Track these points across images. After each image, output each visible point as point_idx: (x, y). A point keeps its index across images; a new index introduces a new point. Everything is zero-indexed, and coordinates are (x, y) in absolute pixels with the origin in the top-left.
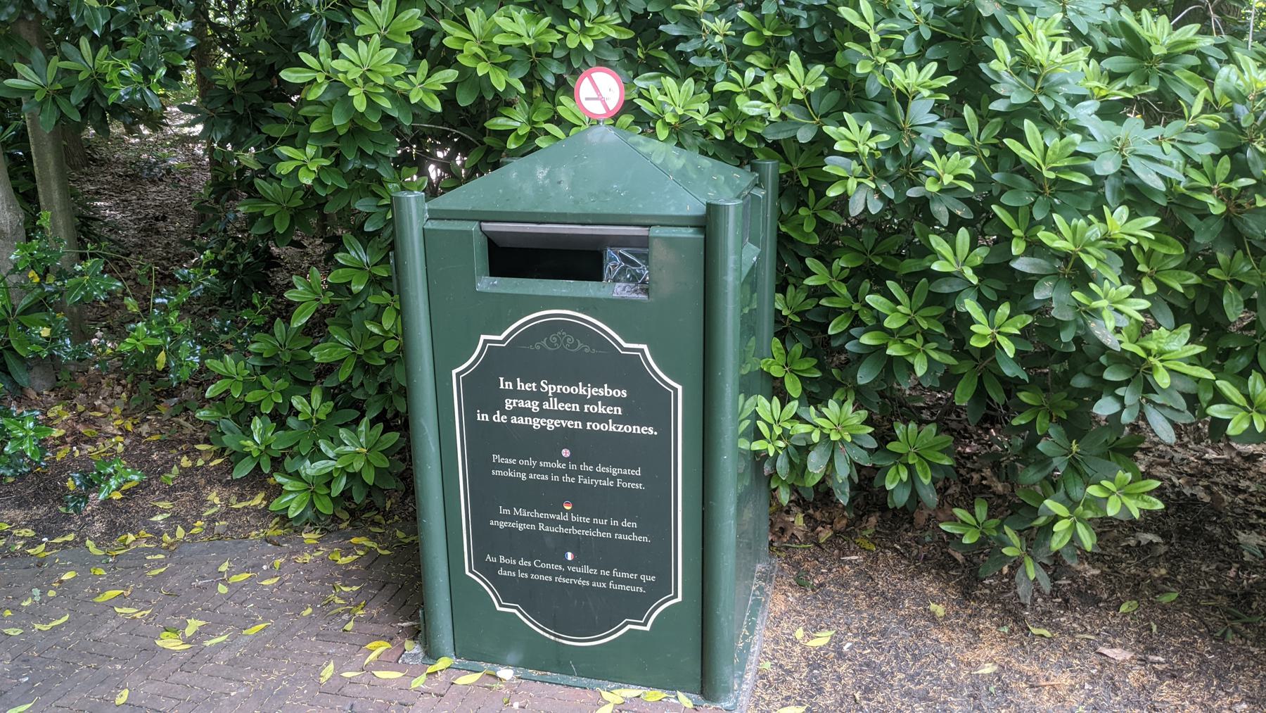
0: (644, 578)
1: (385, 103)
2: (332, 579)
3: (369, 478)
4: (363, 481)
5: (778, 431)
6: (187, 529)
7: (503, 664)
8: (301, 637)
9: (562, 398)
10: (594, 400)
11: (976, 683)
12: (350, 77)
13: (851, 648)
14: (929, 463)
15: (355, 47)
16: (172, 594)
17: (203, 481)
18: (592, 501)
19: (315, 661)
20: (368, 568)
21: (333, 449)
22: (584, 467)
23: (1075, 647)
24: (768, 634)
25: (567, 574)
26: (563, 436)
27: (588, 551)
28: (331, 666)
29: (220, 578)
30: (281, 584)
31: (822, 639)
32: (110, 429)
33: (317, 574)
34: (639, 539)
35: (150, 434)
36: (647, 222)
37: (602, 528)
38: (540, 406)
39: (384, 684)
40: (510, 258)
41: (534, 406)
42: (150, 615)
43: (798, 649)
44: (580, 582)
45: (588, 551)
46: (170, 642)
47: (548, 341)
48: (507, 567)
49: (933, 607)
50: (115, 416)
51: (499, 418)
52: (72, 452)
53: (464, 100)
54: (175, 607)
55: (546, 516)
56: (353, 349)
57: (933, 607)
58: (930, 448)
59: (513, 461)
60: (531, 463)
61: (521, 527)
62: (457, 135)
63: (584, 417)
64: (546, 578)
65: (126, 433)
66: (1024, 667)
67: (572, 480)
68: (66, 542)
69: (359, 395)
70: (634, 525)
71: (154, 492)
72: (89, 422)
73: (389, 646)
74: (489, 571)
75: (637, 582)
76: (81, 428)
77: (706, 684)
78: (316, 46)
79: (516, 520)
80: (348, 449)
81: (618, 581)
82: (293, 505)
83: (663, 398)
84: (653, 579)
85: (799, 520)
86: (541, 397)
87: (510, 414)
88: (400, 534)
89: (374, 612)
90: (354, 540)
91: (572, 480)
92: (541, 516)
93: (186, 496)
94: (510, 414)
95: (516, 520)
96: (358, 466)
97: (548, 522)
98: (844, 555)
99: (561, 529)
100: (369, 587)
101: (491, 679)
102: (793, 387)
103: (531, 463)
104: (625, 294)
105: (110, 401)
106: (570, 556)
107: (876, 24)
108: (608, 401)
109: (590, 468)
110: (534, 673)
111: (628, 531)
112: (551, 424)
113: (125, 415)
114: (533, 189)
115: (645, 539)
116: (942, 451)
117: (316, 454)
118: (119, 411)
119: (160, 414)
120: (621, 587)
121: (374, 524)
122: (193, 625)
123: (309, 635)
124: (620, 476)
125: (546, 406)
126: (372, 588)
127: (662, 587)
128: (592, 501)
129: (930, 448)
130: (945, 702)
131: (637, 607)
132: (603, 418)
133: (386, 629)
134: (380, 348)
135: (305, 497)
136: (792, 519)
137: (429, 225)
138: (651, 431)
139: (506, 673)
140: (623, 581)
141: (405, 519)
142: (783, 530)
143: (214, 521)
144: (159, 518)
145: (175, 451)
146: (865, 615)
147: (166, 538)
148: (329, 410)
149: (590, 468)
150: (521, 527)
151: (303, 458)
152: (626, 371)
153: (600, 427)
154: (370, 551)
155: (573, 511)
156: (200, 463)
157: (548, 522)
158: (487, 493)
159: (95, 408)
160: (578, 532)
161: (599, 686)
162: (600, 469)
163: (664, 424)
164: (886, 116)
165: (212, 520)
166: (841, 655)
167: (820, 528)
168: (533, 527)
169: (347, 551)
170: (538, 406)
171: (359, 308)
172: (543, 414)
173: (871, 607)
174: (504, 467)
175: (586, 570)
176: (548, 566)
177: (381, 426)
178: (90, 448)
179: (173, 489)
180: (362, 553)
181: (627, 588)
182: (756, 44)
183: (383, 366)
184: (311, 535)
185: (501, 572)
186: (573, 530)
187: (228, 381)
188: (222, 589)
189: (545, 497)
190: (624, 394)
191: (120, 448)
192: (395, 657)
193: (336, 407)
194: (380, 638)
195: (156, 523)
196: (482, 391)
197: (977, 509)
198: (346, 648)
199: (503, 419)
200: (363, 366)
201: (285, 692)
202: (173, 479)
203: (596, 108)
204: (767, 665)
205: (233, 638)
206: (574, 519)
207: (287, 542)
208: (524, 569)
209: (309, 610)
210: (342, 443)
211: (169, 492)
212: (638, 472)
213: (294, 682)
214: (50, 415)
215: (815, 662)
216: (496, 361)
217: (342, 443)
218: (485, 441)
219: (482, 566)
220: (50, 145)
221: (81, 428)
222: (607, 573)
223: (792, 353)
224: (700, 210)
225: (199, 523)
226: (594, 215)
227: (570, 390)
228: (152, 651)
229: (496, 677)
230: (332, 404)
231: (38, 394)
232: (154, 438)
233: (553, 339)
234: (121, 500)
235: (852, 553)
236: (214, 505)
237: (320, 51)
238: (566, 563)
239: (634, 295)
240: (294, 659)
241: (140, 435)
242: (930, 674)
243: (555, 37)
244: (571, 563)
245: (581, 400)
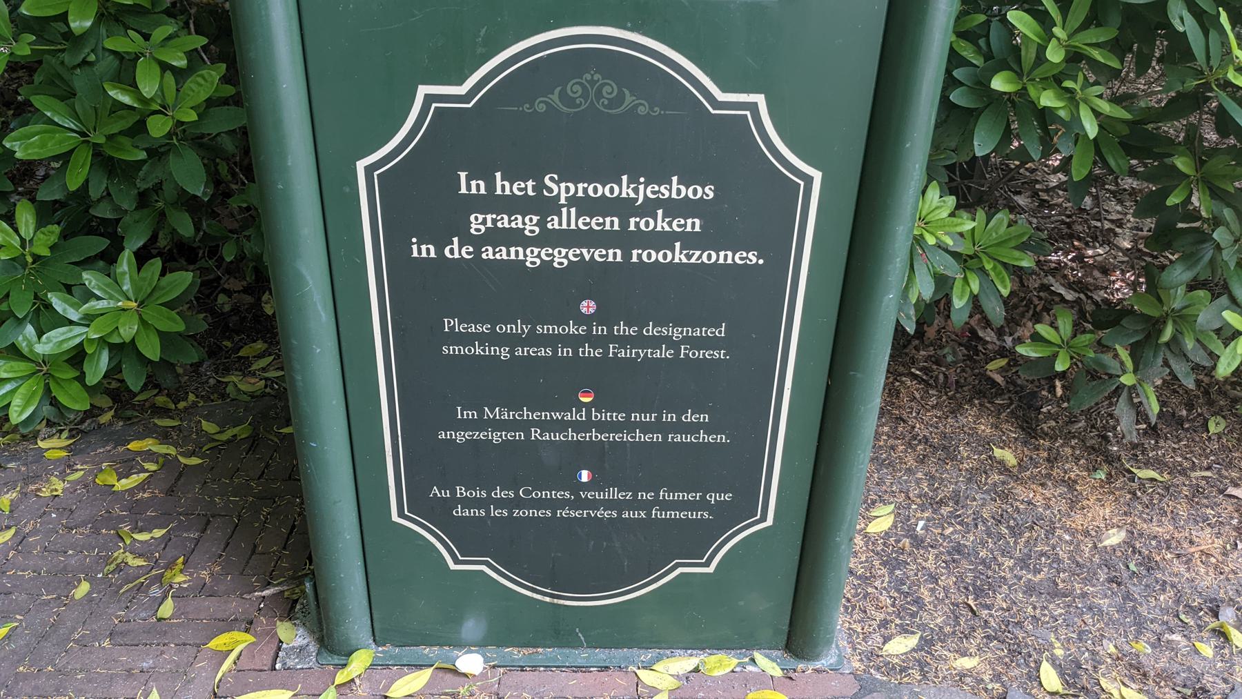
0: (712, 498)
2: (111, 521)
3: (151, 349)
4: (140, 355)
7: (461, 645)
8: (82, 644)
9: (586, 206)
10: (648, 209)
11: (1108, 558)
13: (925, 528)
20: (170, 492)
21: (76, 307)
22: (622, 329)
23: (1197, 491)
25: (578, 504)
26: (585, 278)
27: (611, 464)
33: (81, 515)
37: (646, 428)
38: (542, 224)
41: (529, 225)
45: (611, 464)
47: (563, 96)
48: (467, 503)
49: (998, 453)
51: (456, 250)
56: (83, 134)
57: (998, 453)
59: (485, 328)
60: (519, 328)
61: (496, 437)
63: (625, 240)
66: (1156, 529)
67: (597, 353)
69: (103, 211)
73: (250, 638)
74: (438, 514)
75: (703, 505)
77: (798, 636)
80: (102, 305)
81: (666, 506)
82: (17, 401)
83: (784, 193)
84: (727, 497)
88: (209, 427)
90: (134, 446)
92: (535, 416)
94: (478, 242)
96: (128, 330)
97: (545, 426)
100: (180, 527)
101: (449, 676)
103: (519, 328)
108: (675, 208)
109: (632, 331)
110: (517, 654)
111: (693, 428)
112: (561, 257)
116: (1017, 248)
117: (45, 319)
120: (671, 514)
121: (164, 412)
123: (95, 638)
125: (553, 224)
126: (188, 530)
127: (745, 507)
128: (620, 385)
130: (1084, 595)
131: (694, 541)
132: (663, 241)
133: (234, 606)
134: (140, 128)
135: (34, 386)
138: (752, 257)
139: (471, 663)
141: (207, 399)
146: (920, 475)
148: (53, 239)
149: (632, 331)
150: (496, 437)
151: (20, 322)
152: (719, 149)
153: (657, 256)
154: (167, 463)
155: (597, 405)
157: (545, 426)
158: (431, 387)
160: (602, 437)
162: (651, 330)
163: (778, 250)
166: (918, 542)
169: (127, 466)
170: (540, 223)
171: (85, 63)
172: (547, 238)
173: (922, 460)
174: (467, 339)
175: (614, 494)
176: (544, 494)
177: (156, 264)
180: (152, 467)
183: (143, 162)
184: (54, 442)
185: (459, 512)
189: (547, 384)
192: (267, 660)
193: (64, 236)
194: (228, 625)
196: (419, 198)
197: (1060, 323)
198: (171, 654)
199: (466, 252)
200: (104, 162)
207: (13, 458)
208: (500, 503)
209: (84, 587)
210: (89, 296)
212: (721, 332)
216: (451, 136)
217: (89, 296)
218: (422, 297)
219: (419, 504)
227: (604, 190)
229: (455, 672)
230: (56, 229)
233: (574, 89)
238: (578, 487)
244: (586, 487)
245: (623, 208)
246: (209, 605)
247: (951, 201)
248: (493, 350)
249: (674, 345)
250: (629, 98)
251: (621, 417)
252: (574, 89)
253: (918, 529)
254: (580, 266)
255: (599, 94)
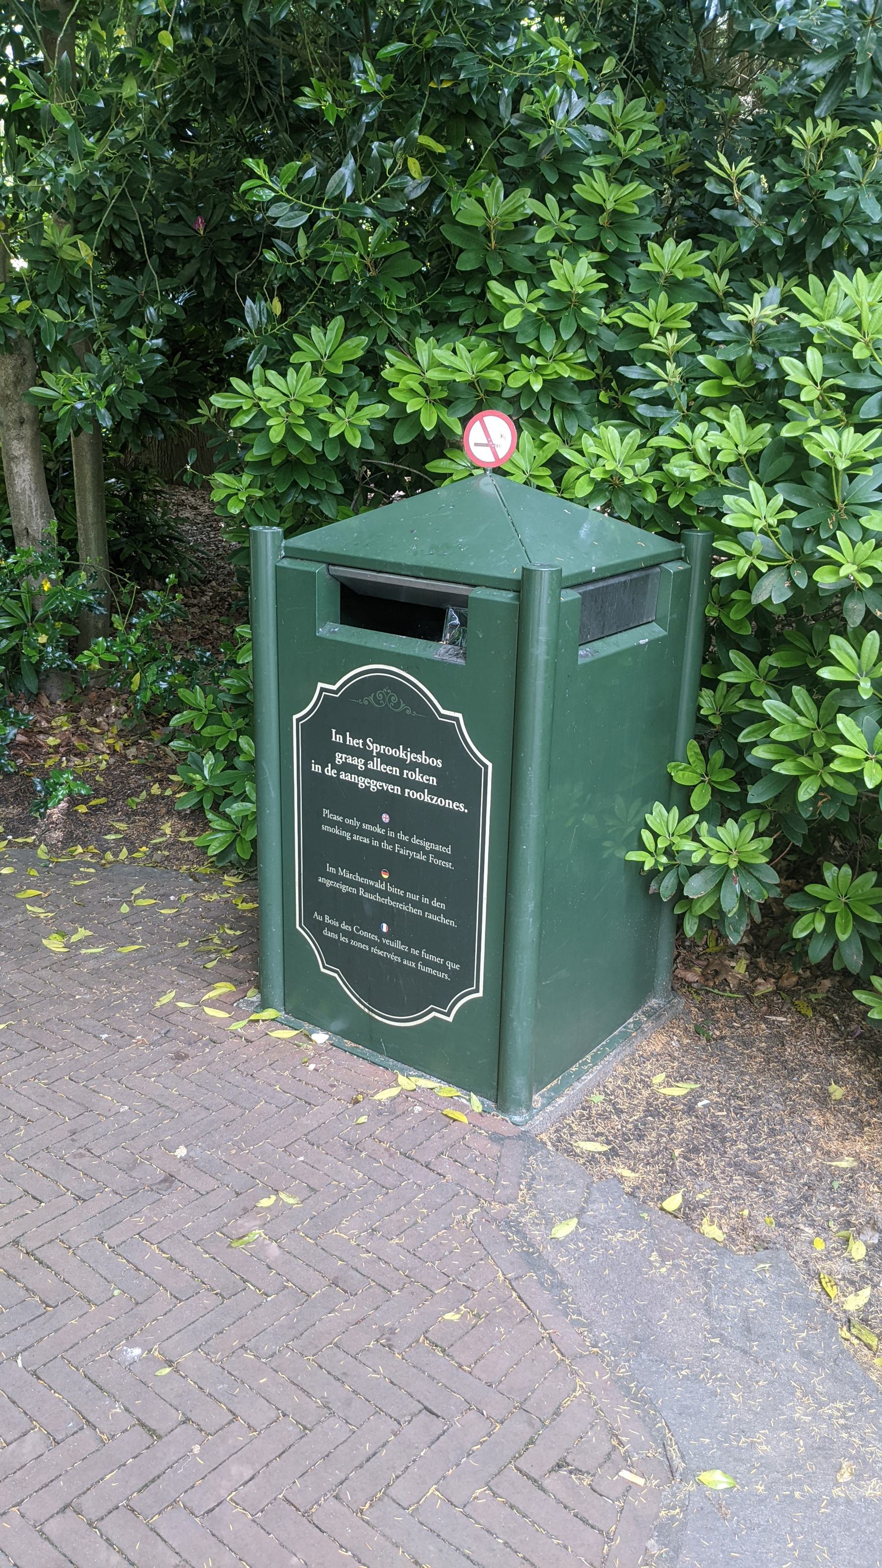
0: (450, 965)
1: (306, 435)
5: (662, 844)
6: (131, 852)
7: (324, 1029)
9: (387, 760)
10: (412, 766)
12: (270, 405)
14: (856, 917)
15: (284, 375)
16: (82, 905)
17: (164, 810)
18: (409, 874)
19: (162, 987)
24: (620, 1069)
26: (384, 800)
27: (403, 928)
28: (173, 994)
29: (128, 898)
30: (177, 915)
31: (680, 1090)
32: (100, 746)
33: (213, 913)
34: (446, 922)
35: (135, 757)
36: (473, 582)
37: (415, 904)
38: (365, 764)
39: (208, 1020)
40: (373, 606)
41: (359, 763)
42: (52, 918)
43: (646, 1093)
44: (393, 957)
45: (403, 928)
46: (55, 944)
47: (375, 697)
48: (332, 928)
50: (110, 735)
51: (330, 772)
52: (61, 762)
53: (401, 438)
54: (74, 911)
55: (366, 881)
58: (862, 901)
59: (340, 819)
61: (344, 888)
62: (409, 474)
64: (363, 946)
65: (113, 753)
67: (390, 848)
68: (26, 843)
70: (443, 906)
71: (116, 813)
72: (84, 736)
74: (316, 928)
75: (442, 968)
76: (75, 741)
78: (251, 372)
79: (341, 880)
81: (427, 963)
83: (474, 772)
84: (457, 967)
85: (740, 967)
86: (367, 755)
87: (340, 768)
89: (241, 957)
91: (390, 848)
92: (361, 880)
93: (142, 822)
94: (340, 768)
95: (341, 880)
98: (771, 1014)
99: (379, 899)
102: (700, 800)
104: (446, 658)
105: (111, 720)
106: (385, 928)
107: (824, 379)
108: (426, 770)
109: (406, 838)
110: (349, 1044)
113: (120, 735)
114: (391, 537)
115: (452, 923)
118: (115, 732)
119: (151, 740)
122: (82, 933)
123: (172, 964)
124: (432, 851)
125: (370, 766)
128: (409, 874)
129: (862, 901)
131: (442, 995)
132: (419, 787)
136: (733, 964)
137: (286, 563)
138: (462, 808)
139: (320, 1037)
140: (431, 964)
142: (717, 973)
143: (158, 849)
144: (111, 837)
145: (149, 778)
147: (109, 856)
149: (406, 838)
150: (344, 888)
152: (441, 739)
156: (168, 792)
158: (321, 851)
159: (95, 725)
160: (393, 903)
161: (402, 1072)
162: (415, 841)
163: (473, 801)
164: (823, 490)
165: (156, 848)
167: (760, 980)
168: (354, 891)
170: (368, 764)
174: (333, 824)
175: (398, 945)
176: (365, 934)
178: (77, 761)
179: (135, 813)
181: (434, 972)
182: (714, 394)
185: (326, 932)
186: (388, 901)
187: (195, 713)
188: (125, 909)
189: (367, 861)
190: (439, 763)
191: (103, 765)
194: (230, 980)
195: (106, 841)
201: (121, 1006)
202: (138, 804)
203: (484, 455)
204: (597, 1098)
205: (108, 952)
206: (391, 889)
211: (129, 815)
212: (448, 850)
213: (135, 1000)
214: (53, 724)
215: (655, 1109)
216: (333, 712)
218: (320, 793)
220: (88, 455)
221: (75, 741)
222: (416, 952)
223: (711, 761)
224: (515, 573)
225: (144, 849)
226: (445, 571)
227: (392, 752)
228: (36, 947)
231: (51, 703)
232: (136, 761)
234: (86, 814)
235: (782, 1014)
236: (164, 834)
237: (254, 377)
238: (378, 932)
239: (455, 659)
240: (146, 981)
241: (126, 757)
242: (777, 1153)
243: (496, 375)
245: (400, 763)
246: (230, 970)
247: (846, 870)
248: (343, 833)
249: (426, 853)
250: (402, 705)
251: (401, 893)
252: (380, 696)
253: (700, 1104)
254: (381, 792)
255: (390, 701)
